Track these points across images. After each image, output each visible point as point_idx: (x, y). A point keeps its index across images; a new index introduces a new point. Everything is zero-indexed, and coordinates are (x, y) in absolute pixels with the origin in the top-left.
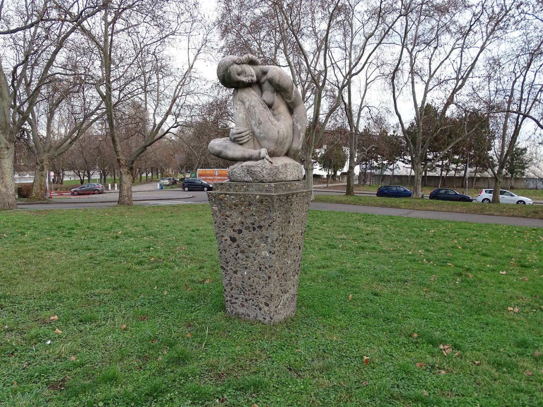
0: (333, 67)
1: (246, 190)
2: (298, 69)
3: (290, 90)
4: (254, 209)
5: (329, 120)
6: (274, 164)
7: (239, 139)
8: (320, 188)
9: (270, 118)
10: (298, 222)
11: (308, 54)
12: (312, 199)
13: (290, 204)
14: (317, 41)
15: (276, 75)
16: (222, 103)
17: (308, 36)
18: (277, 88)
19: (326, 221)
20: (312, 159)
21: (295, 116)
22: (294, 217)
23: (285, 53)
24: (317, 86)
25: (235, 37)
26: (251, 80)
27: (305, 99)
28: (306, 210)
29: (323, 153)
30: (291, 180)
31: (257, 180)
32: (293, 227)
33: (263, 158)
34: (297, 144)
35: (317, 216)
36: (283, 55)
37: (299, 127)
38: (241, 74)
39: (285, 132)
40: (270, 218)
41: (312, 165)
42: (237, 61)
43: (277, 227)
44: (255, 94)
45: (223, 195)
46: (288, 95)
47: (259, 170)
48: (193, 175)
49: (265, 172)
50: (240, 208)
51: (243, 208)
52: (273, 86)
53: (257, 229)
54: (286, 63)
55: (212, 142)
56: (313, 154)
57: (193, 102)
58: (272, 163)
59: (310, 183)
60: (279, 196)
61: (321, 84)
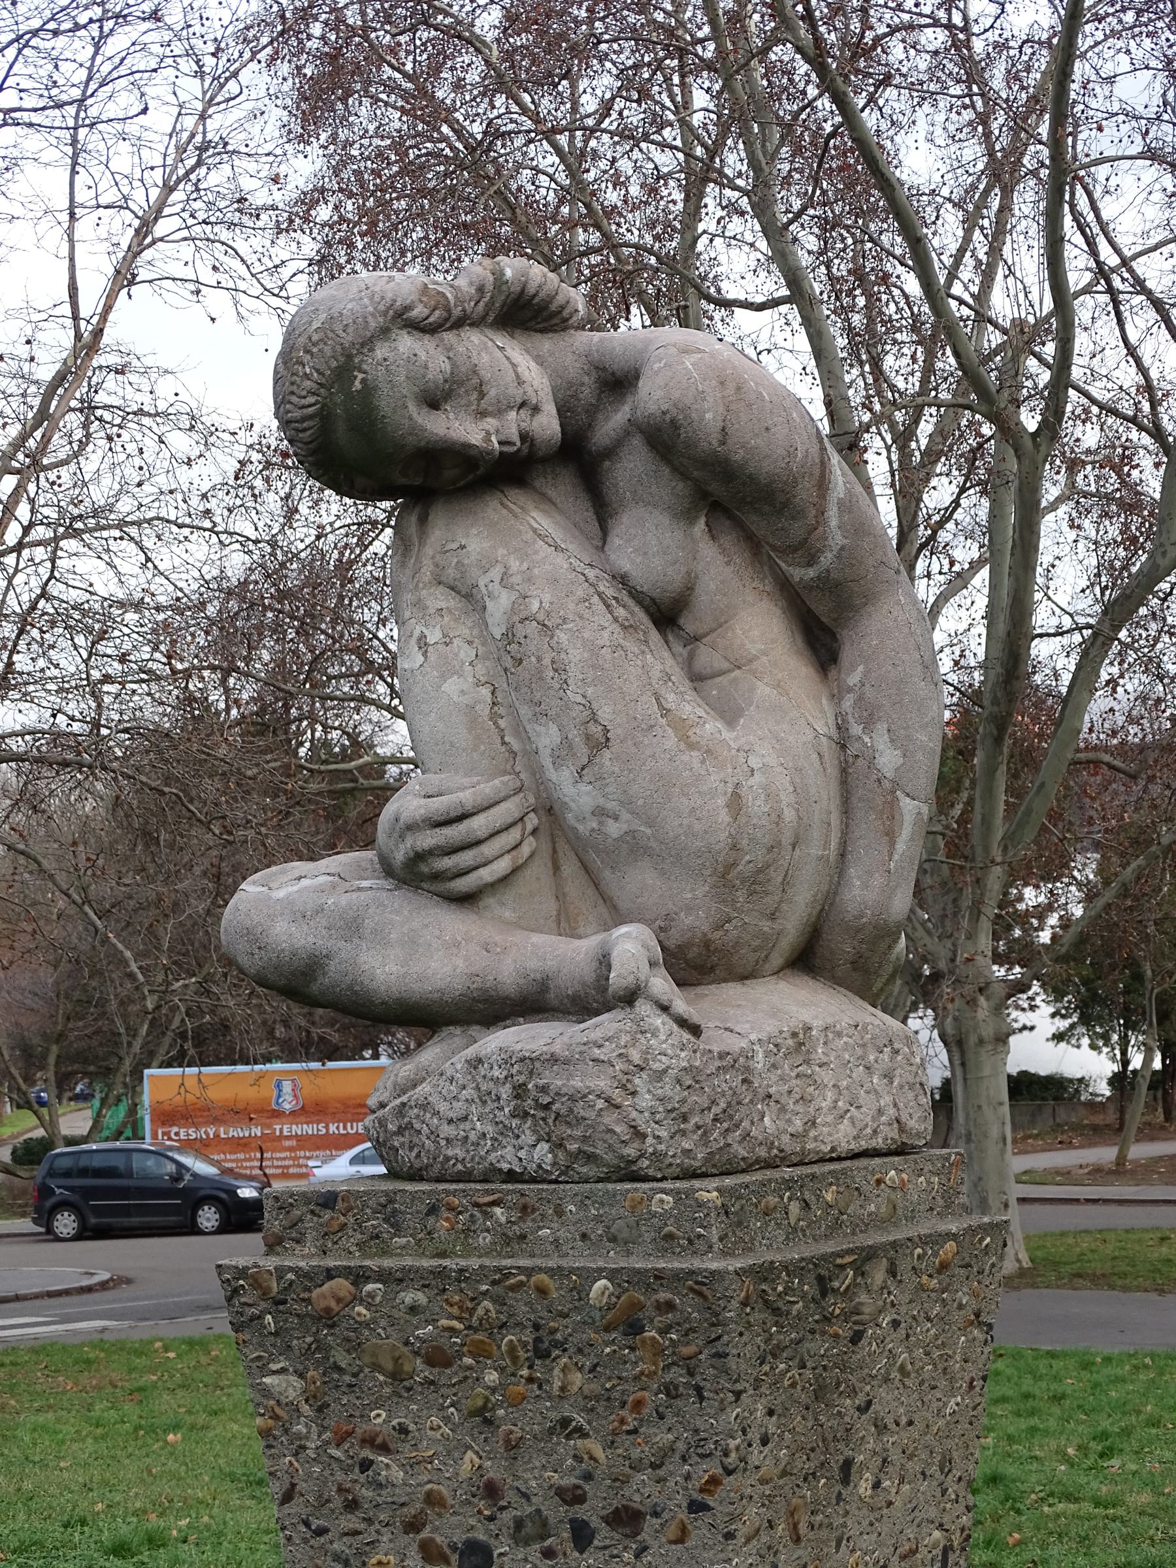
0: (1111, 290)
1: (507, 1240)
2: (857, 319)
3: (805, 492)
4: (577, 1378)
5: (1106, 672)
6: (716, 1041)
7: (447, 863)
8: (1065, 1176)
9: (671, 699)
10: (914, 1467)
11: (930, 214)
12: (1009, 1267)
13: (844, 1331)
14: (984, 119)
15: (701, 395)
16: (314, 581)
17: (923, 95)
18: (716, 488)
19: (1126, 1432)
20: (998, 959)
21: (853, 679)
22: (881, 1428)
23: (762, 209)
24: (1008, 430)
25: (395, 121)
26: (524, 436)
27: (923, 532)
28: (973, 1370)
29: (1078, 911)
30: (844, 1147)
31: (591, 1158)
32: (879, 1507)
33: (629, 998)
34: (878, 881)
35: (1058, 1398)
36: (747, 227)
37: (888, 759)
38: (448, 395)
39: (786, 798)
40: (698, 1449)
41: (999, 1009)
42: (418, 312)
43: (753, 1514)
44: (558, 535)
45: (341, 1285)
46: (797, 530)
47: (602, 1083)
48: (115, 1116)
49: (645, 1100)
50: (469, 1379)
51: (492, 1377)
52: (681, 473)
53: (604, 1535)
54: (772, 285)
55: (250, 888)
56: (1001, 927)
57: (107, 585)
58: (695, 1030)
59: (992, 1148)
60: (763, 1273)
61: (1030, 421)
